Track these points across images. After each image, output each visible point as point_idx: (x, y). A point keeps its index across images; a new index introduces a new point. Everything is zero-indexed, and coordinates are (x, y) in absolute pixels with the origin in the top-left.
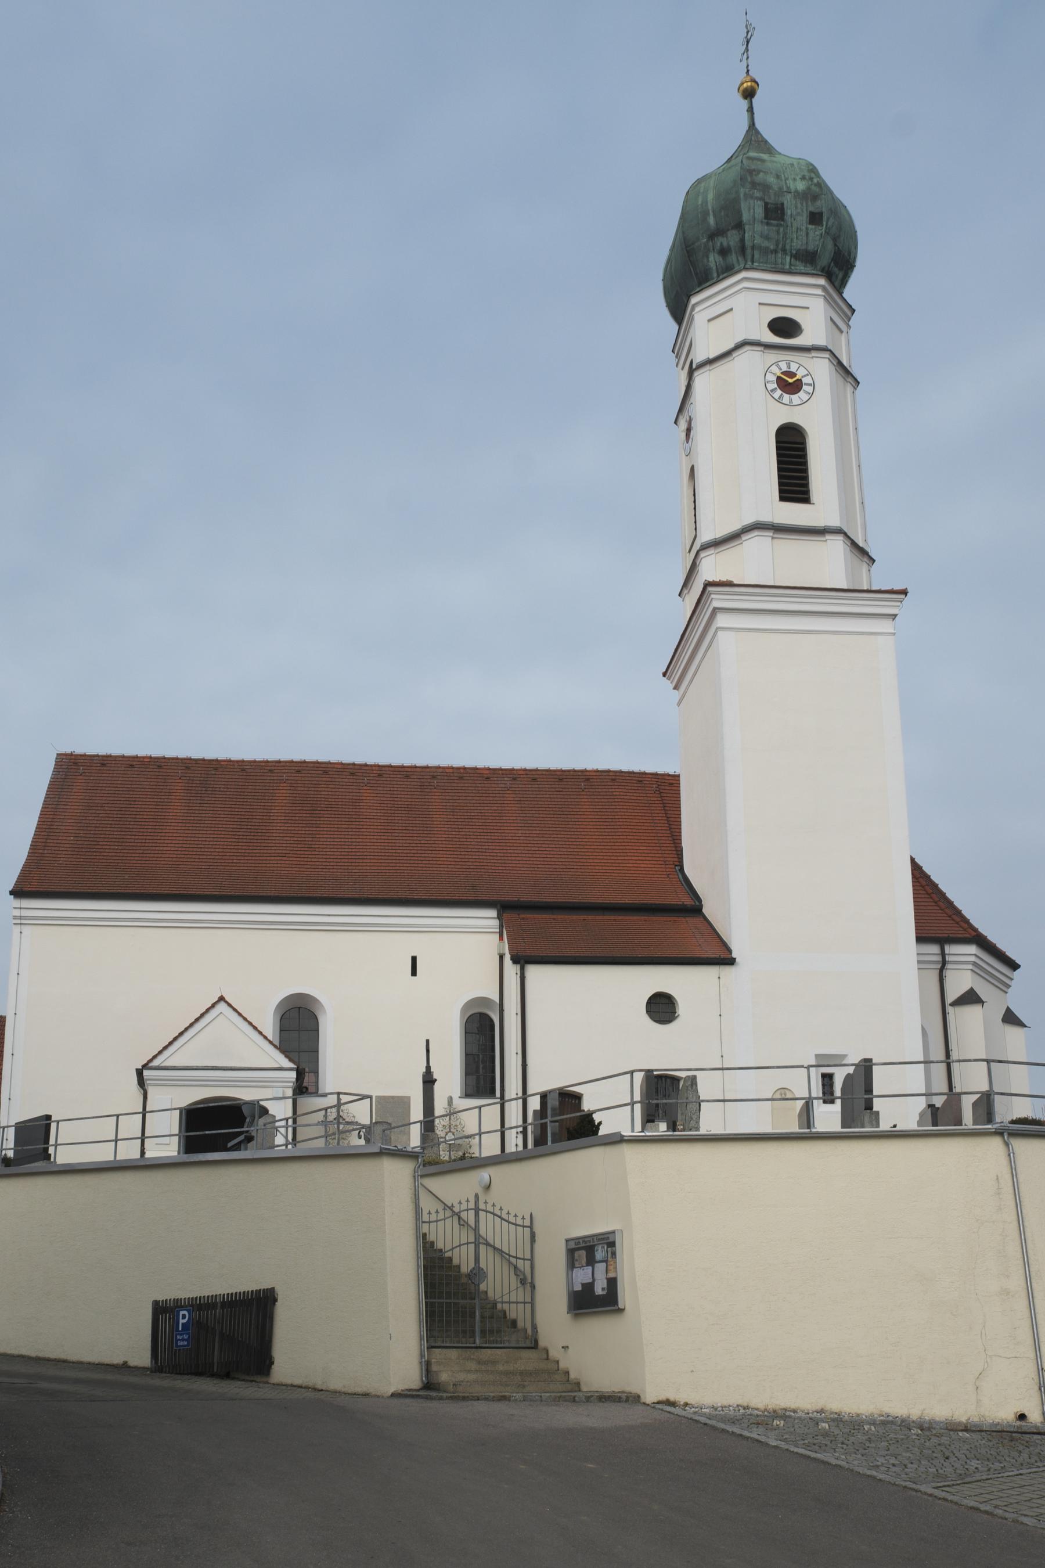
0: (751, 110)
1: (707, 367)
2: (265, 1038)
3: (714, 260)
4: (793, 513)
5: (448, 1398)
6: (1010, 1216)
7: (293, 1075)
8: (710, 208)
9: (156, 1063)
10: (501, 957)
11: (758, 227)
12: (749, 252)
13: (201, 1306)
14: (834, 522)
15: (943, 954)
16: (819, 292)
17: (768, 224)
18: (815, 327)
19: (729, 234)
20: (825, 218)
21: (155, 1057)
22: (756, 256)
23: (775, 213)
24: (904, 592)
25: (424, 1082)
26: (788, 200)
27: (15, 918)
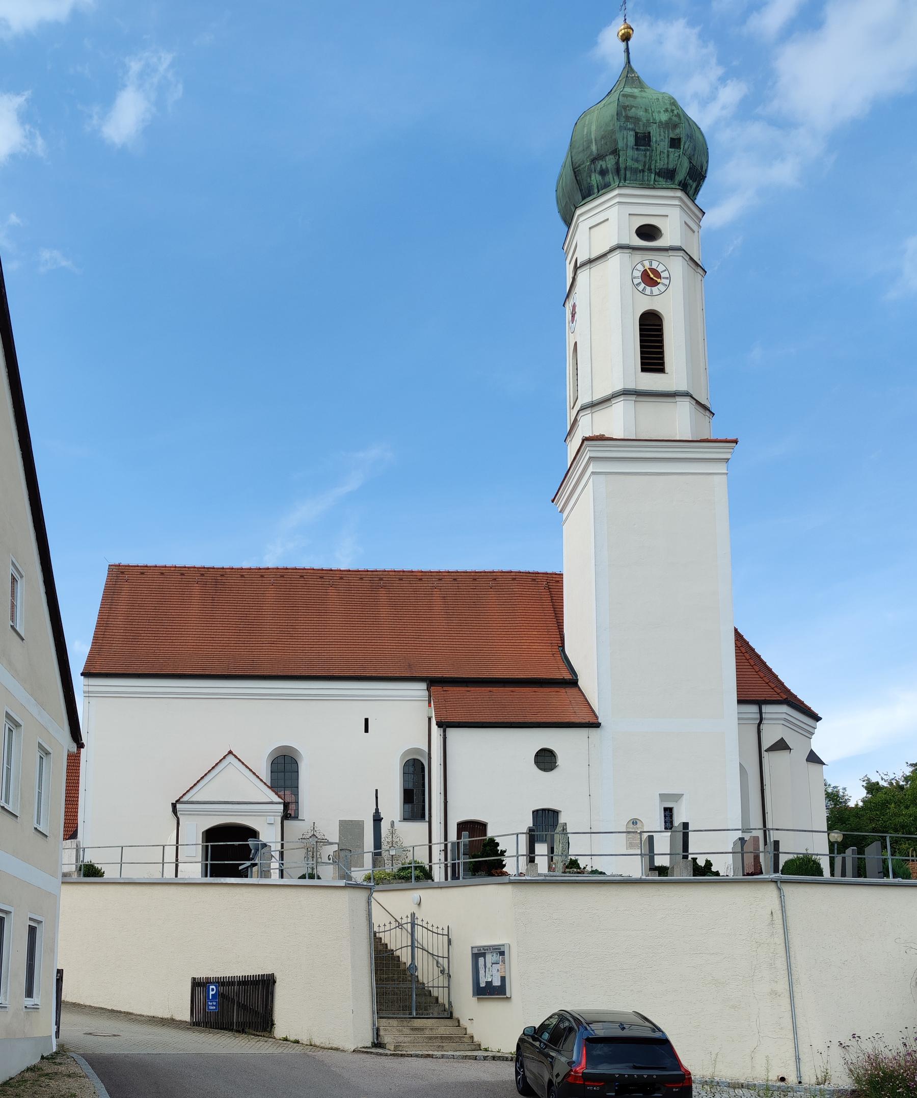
0: (627, 50)
1: (588, 266)
2: (261, 780)
3: (595, 179)
4: (651, 381)
5: (391, 1055)
6: (779, 940)
7: (281, 807)
8: (593, 137)
9: (185, 799)
10: (430, 719)
11: (630, 153)
12: (622, 172)
13: (222, 983)
14: (683, 387)
15: (761, 713)
16: (677, 202)
17: (637, 149)
18: (672, 231)
19: (607, 158)
20: (682, 143)
21: (184, 795)
22: (628, 175)
23: (643, 140)
24: (736, 442)
25: (374, 820)
26: (654, 130)
27: (84, 692)
